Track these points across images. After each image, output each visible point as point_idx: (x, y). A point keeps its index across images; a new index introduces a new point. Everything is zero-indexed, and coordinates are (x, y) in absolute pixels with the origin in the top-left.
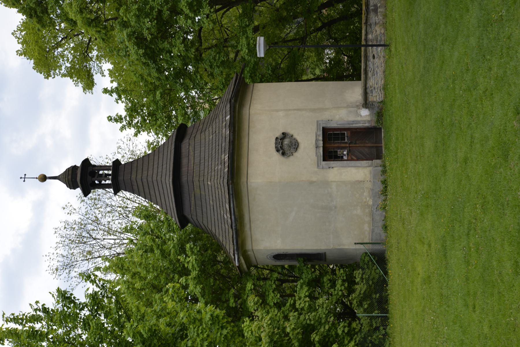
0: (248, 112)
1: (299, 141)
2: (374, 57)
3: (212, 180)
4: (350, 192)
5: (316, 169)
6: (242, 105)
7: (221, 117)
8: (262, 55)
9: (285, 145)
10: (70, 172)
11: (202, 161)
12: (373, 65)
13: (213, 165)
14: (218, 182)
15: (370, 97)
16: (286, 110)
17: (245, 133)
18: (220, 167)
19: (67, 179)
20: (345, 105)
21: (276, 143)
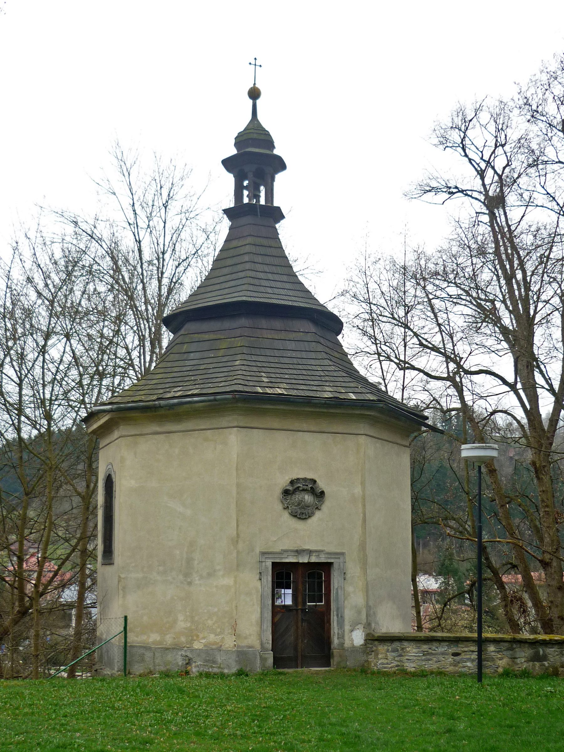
0: (362, 432)
1: (310, 521)
2: (456, 654)
3: (243, 368)
4: (216, 610)
5: (258, 550)
6: (374, 421)
7: (352, 385)
8: (464, 454)
9: (303, 497)
10: (262, 137)
11: (277, 353)
12: (443, 654)
13: (269, 370)
14: (239, 377)
15: (386, 648)
16: (364, 498)
17: (324, 425)
18: (265, 380)
19: (252, 131)
20: (373, 601)
21: (305, 480)
